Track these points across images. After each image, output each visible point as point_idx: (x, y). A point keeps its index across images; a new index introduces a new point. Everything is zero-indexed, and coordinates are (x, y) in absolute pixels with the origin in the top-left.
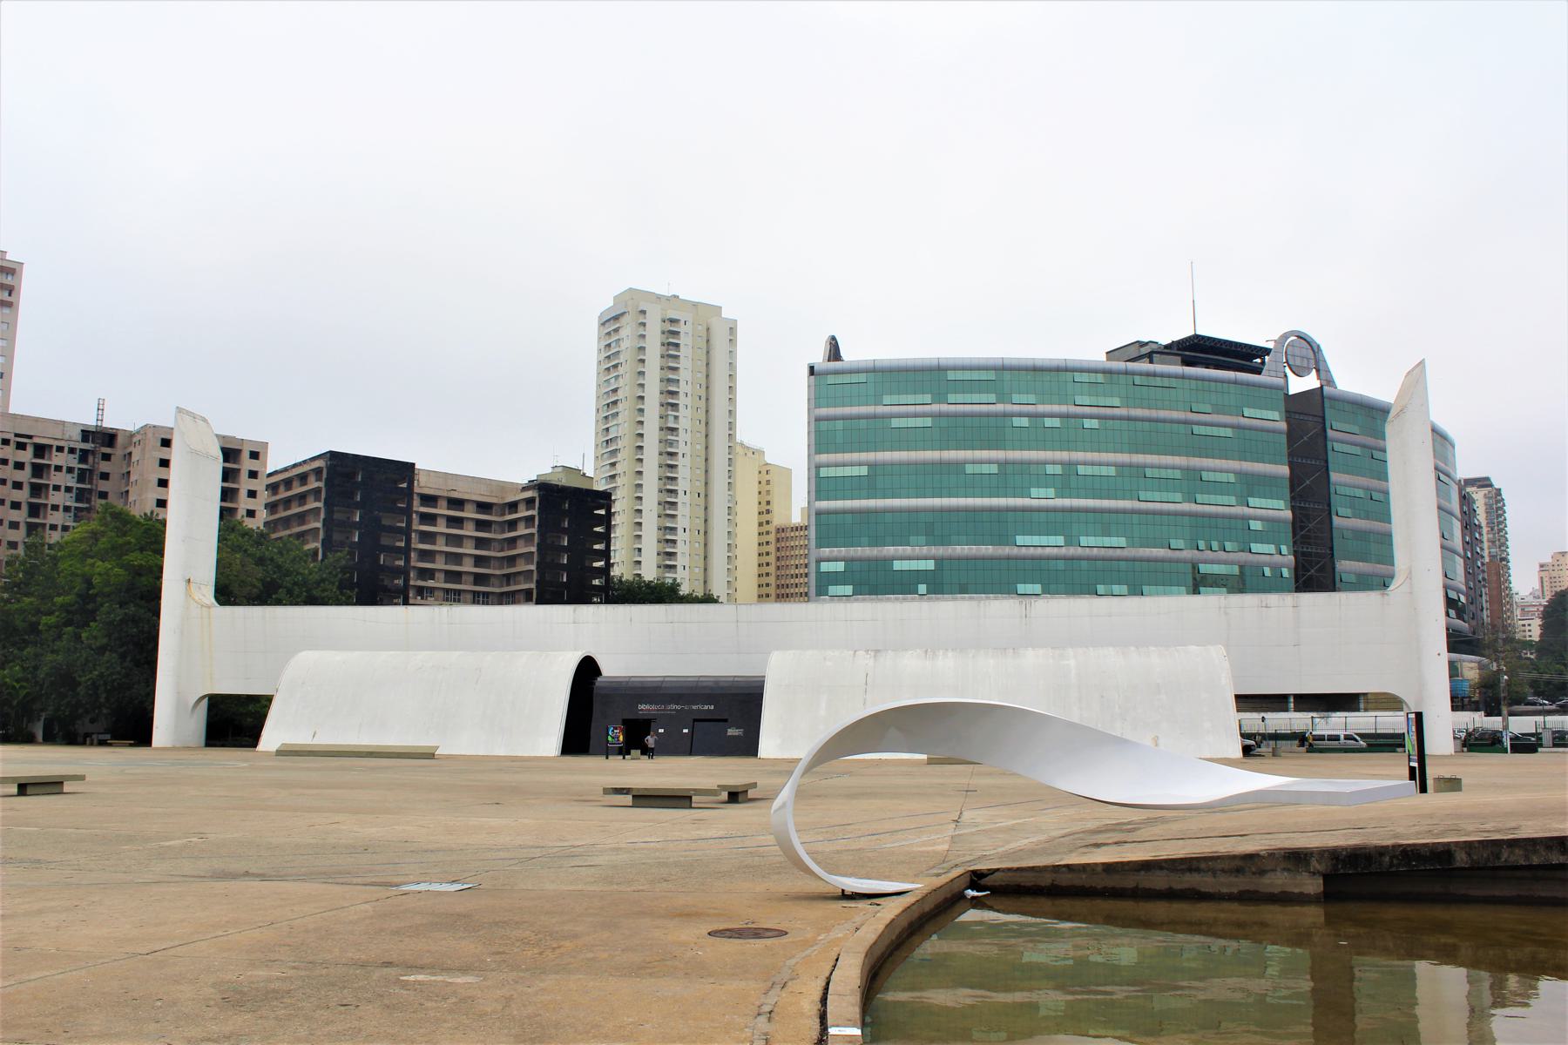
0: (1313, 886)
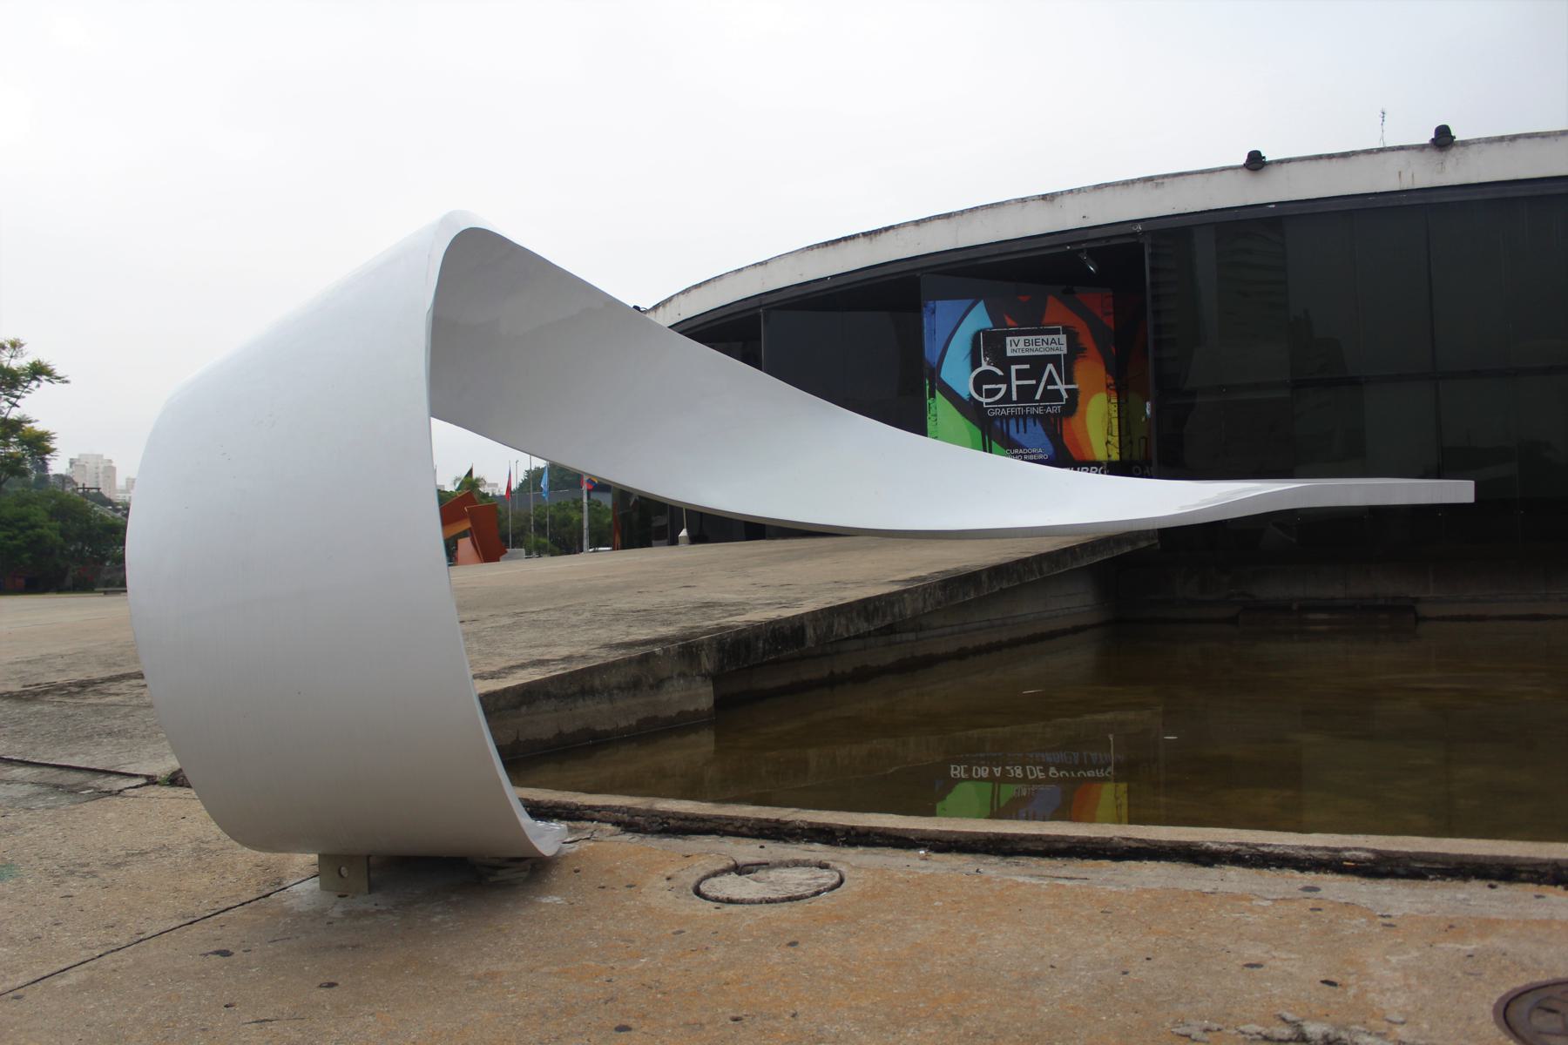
0: (702, 697)
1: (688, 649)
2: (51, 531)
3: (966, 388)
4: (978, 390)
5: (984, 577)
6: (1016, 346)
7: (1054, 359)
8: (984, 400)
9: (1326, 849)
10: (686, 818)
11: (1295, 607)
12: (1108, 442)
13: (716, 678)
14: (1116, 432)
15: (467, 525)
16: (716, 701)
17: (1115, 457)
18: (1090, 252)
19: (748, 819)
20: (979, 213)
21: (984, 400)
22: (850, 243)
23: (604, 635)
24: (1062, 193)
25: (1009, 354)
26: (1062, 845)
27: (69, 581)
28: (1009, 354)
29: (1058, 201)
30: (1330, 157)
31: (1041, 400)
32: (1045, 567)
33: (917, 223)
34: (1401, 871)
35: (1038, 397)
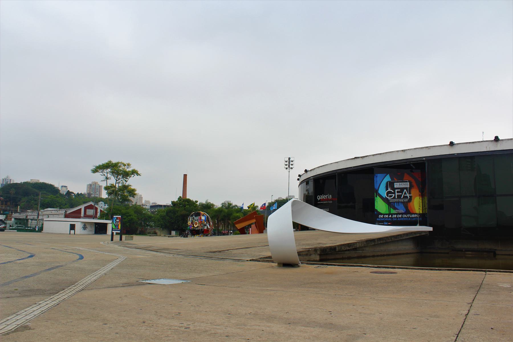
1: (315, 250)
2: (134, 217)
3: (384, 195)
4: (388, 196)
6: (397, 185)
7: (406, 188)
13: (320, 255)
15: (254, 221)
17: (421, 212)
18: (413, 164)
23: (301, 247)
27: (138, 232)
32: (392, 239)
33: (373, 155)
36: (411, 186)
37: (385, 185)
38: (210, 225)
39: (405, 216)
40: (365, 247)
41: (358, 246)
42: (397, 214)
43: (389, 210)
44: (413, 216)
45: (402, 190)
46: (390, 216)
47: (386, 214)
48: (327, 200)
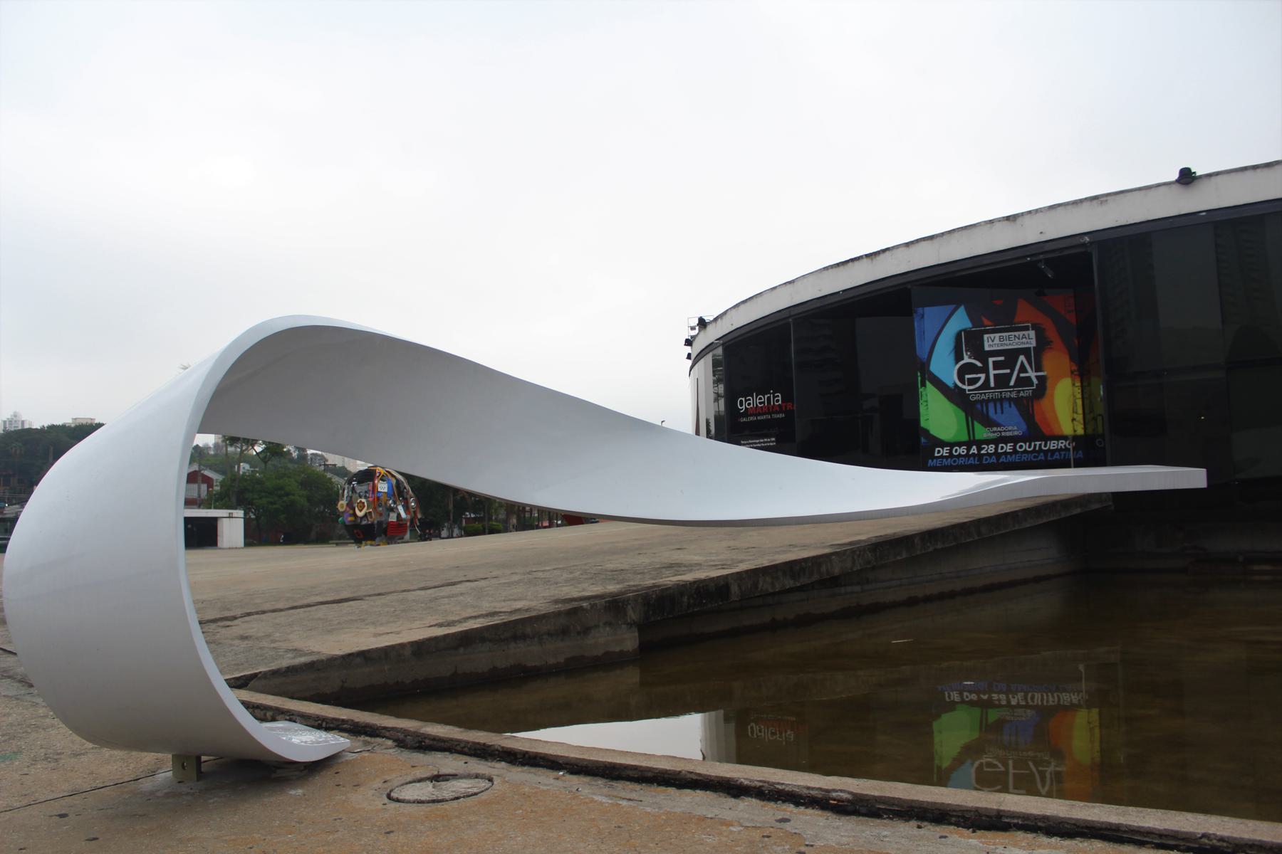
0: (629, 641)
1: (614, 606)
3: (951, 378)
4: (961, 379)
5: (916, 540)
6: (992, 342)
7: (1025, 351)
8: (966, 387)
9: (820, 789)
10: (434, 739)
11: (1241, 559)
12: (1073, 420)
13: (642, 627)
14: (1080, 411)
16: (641, 644)
17: (1080, 431)
18: (1047, 261)
19: (468, 742)
20: (956, 234)
21: (966, 387)
22: (856, 263)
24: (1022, 214)
25: (987, 348)
26: (650, 774)
27: (313, 534)
28: (987, 348)
29: (1019, 220)
30: (1255, 167)
31: (1016, 385)
33: (907, 245)
34: (863, 810)
35: (1012, 383)
36: (1043, 343)
37: (951, 345)
38: (407, 508)
39: (1025, 446)
40: (874, 568)
41: (836, 571)
42: (996, 442)
43: (970, 430)
44: (1053, 445)
45: (1010, 357)
46: (974, 450)
47: (960, 444)
48: (770, 410)
